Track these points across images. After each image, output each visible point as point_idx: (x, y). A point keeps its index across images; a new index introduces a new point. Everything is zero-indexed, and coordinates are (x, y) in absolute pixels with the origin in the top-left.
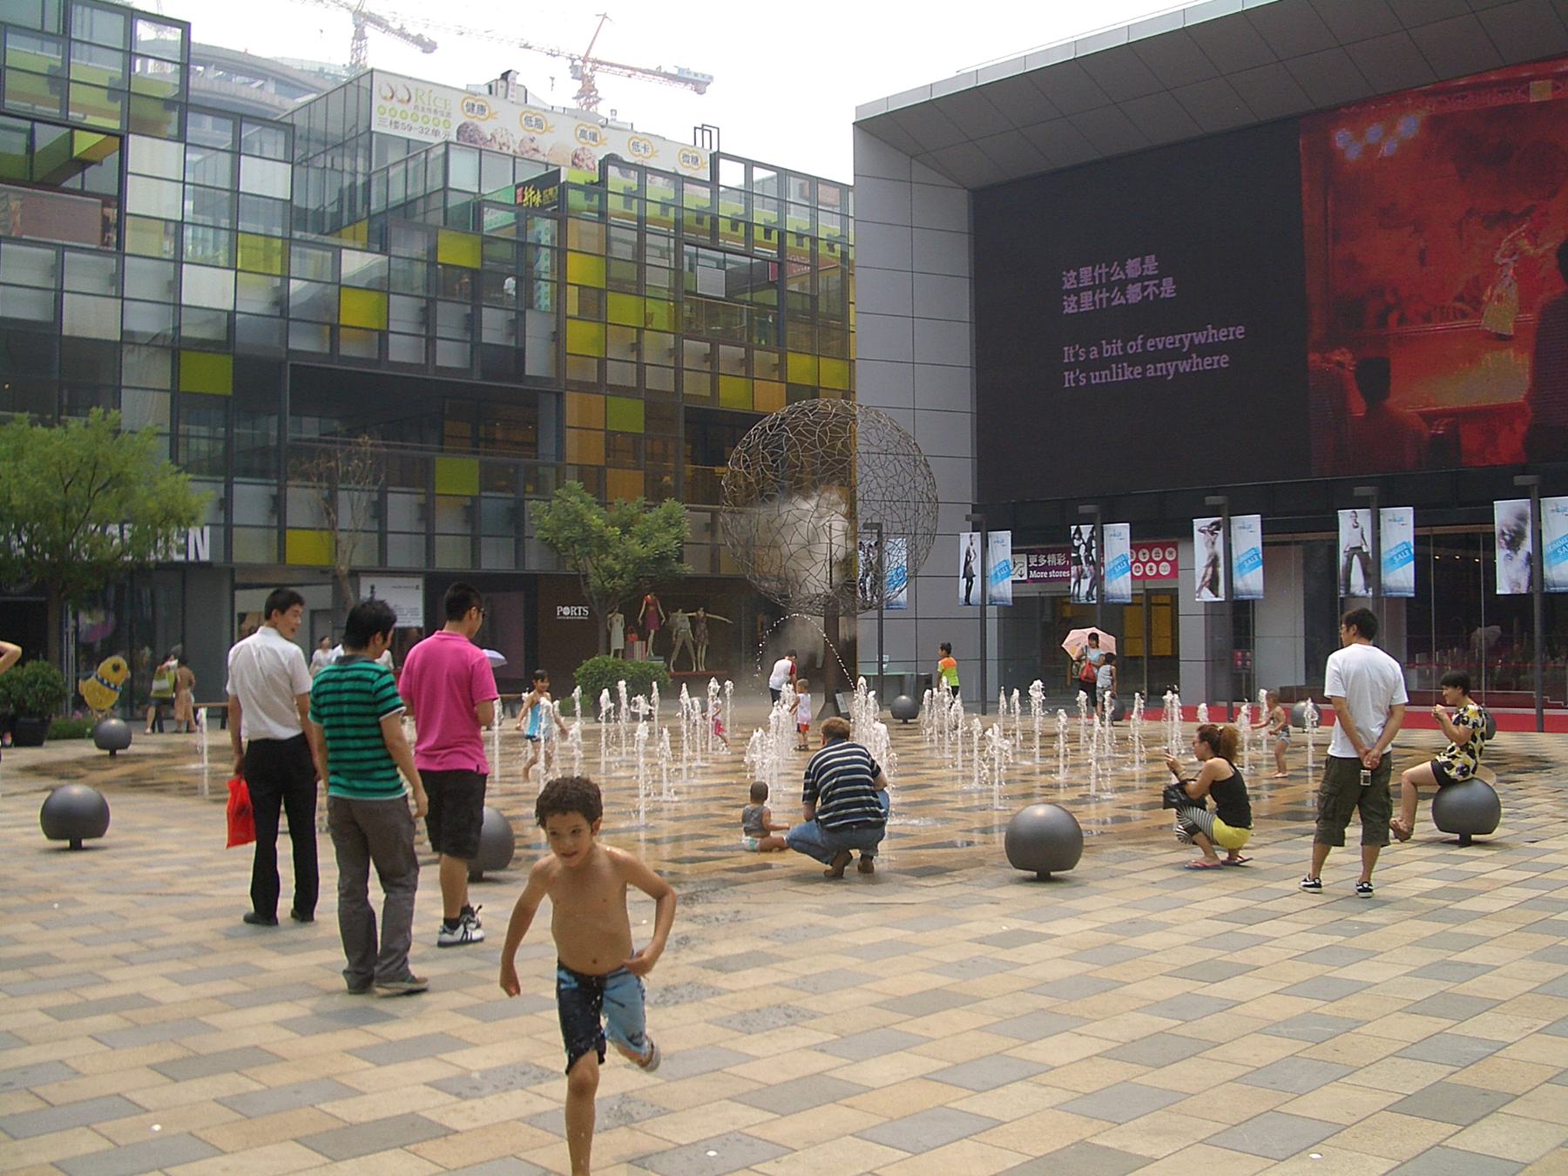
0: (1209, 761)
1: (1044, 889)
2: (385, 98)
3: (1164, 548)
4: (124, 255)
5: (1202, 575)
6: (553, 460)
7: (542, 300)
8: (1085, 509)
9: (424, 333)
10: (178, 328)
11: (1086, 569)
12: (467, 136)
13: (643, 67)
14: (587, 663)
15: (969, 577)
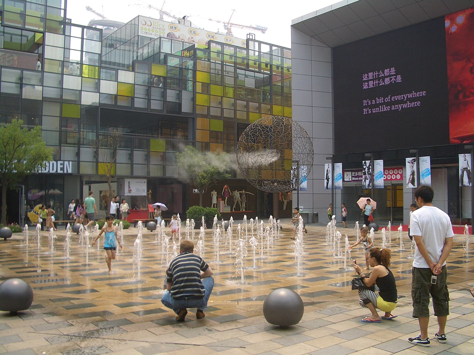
0: (376, 267)
1: (278, 336)
2: (143, 25)
3: (398, 169)
4: (44, 72)
5: (409, 178)
6: (191, 140)
7: (189, 87)
8: (367, 155)
9: (147, 98)
10: (62, 96)
11: (368, 176)
12: (171, 37)
13: (246, 25)
14: (190, 208)
15: (328, 179)
